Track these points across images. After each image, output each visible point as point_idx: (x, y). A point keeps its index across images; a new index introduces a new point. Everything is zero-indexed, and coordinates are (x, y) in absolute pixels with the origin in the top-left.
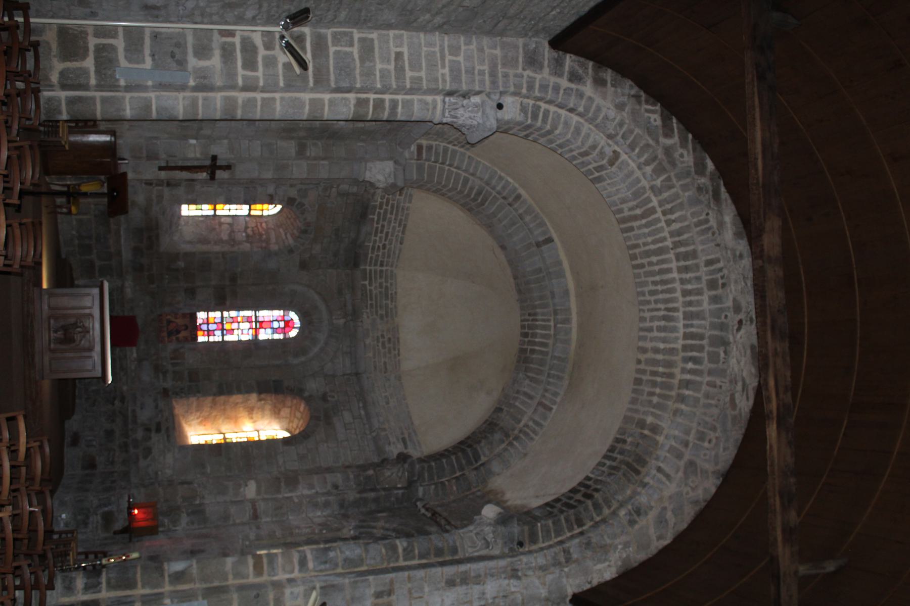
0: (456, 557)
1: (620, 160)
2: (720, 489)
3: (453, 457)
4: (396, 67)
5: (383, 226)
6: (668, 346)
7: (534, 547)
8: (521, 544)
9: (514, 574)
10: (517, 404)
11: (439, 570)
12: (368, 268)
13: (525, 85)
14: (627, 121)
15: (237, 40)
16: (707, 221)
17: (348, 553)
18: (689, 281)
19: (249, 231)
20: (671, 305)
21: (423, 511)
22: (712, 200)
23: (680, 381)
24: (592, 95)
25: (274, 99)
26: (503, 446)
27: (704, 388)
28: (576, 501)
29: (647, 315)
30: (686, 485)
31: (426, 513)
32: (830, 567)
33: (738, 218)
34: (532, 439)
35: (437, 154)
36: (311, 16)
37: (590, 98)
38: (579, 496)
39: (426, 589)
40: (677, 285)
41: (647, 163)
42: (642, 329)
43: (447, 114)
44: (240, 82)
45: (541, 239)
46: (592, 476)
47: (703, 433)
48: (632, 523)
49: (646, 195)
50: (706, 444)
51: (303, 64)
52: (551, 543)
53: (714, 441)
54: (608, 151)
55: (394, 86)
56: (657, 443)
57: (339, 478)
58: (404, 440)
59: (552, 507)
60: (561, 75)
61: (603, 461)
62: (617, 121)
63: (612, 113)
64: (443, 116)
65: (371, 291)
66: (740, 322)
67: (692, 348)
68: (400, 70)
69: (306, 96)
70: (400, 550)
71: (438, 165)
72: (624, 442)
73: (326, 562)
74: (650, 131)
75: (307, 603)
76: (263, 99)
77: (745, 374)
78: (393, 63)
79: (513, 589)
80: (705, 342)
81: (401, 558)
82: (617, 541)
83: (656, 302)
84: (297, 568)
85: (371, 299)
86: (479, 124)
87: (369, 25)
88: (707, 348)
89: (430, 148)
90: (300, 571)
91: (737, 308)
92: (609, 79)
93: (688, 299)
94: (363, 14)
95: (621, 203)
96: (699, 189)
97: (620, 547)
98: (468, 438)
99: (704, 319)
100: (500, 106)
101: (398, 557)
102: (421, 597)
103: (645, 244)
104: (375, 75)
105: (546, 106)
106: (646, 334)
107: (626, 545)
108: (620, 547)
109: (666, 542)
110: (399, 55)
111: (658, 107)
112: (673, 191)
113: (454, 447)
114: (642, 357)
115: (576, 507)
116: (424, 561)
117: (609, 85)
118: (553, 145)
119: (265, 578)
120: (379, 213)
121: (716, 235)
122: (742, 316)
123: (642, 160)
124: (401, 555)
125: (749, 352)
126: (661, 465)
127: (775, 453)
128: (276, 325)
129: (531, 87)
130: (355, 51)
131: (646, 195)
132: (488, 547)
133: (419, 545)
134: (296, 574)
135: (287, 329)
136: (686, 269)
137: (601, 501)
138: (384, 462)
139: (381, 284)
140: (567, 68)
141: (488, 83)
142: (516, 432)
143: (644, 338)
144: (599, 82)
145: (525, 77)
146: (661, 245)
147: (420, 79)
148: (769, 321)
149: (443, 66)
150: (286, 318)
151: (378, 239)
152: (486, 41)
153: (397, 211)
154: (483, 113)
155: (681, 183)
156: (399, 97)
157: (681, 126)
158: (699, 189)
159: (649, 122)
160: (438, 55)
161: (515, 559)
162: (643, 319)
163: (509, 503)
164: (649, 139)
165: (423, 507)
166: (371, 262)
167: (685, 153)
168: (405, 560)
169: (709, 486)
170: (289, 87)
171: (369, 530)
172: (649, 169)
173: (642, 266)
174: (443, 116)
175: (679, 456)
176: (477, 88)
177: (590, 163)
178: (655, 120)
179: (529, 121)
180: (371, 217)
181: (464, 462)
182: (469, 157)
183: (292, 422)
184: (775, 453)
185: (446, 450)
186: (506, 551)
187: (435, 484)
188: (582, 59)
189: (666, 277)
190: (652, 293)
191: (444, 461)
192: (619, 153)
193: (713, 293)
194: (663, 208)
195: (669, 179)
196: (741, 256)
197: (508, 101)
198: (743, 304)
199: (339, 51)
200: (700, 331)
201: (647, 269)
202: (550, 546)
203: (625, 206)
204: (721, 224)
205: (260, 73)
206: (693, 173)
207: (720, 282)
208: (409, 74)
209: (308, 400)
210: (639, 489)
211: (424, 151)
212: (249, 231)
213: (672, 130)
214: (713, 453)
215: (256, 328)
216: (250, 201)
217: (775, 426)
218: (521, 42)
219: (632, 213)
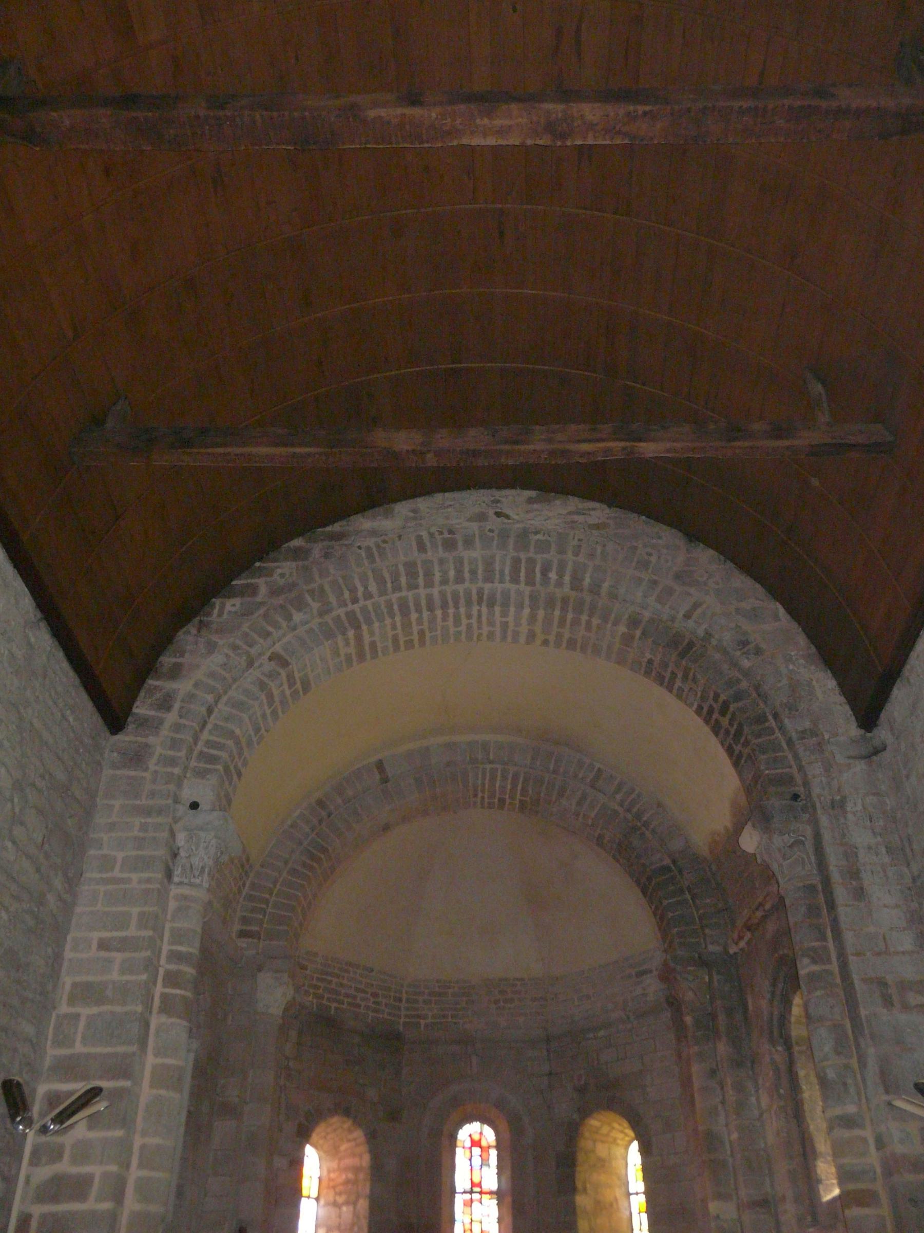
0: (820, 887)
1: (283, 653)
2: (709, 545)
3: (665, 903)
4: (118, 950)
5: (347, 996)
6: (527, 602)
7: (798, 779)
8: (796, 797)
9: (838, 805)
10: (593, 815)
11: (841, 911)
12: (402, 1020)
13: (169, 769)
14: (232, 640)
15: (37, 1210)
16: (368, 549)
17: (827, 1049)
18: (445, 573)
19: (340, 1200)
20: (475, 597)
21: (742, 944)
22: (341, 542)
23: (572, 589)
24: (192, 682)
25: (143, 1147)
26: (648, 834)
27: (581, 559)
28: (731, 724)
29: (485, 629)
30: (705, 584)
31: (746, 939)
32: (817, 388)
33: (366, 513)
34: (639, 795)
35: (253, 910)
36: (17, 1078)
37: (196, 685)
38: (725, 722)
39: (872, 929)
40: (448, 589)
41: (289, 617)
42: (504, 638)
43: (198, 881)
44: (107, 1206)
45: (378, 777)
46: (695, 706)
47: (638, 562)
48: (758, 651)
49: (330, 622)
50: (653, 559)
51: (94, 1093)
52: (790, 757)
53: (649, 550)
54: (269, 667)
55: (148, 953)
56: (651, 621)
57: (696, 1069)
58: (640, 974)
59: (740, 756)
60: (161, 722)
61: (675, 691)
62: (230, 653)
63: (218, 658)
64: (199, 886)
65: (434, 1016)
66: (498, 514)
67: (530, 572)
68: (125, 944)
69: (146, 1093)
70: (816, 968)
71: (270, 910)
72: (650, 662)
73: (845, 1084)
74: (247, 613)
75: (913, 1116)
76: (141, 1166)
77: (565, 512)
78: (114, 954)
79: (859, 807)
80: (523, 556)
81: (827, 967)
82: (784, 670)
83: (469, 616)
84: (857, 1132)
85: (444, 1016)
86: (215, 837)
87: (50, 987)
88: (531, 555)
89: (244, 920)
90: (862, 1126)
91: (481, 517)
92: (173, 660)
93: (467, 575)
94: (31, 996)
95: (339, 655)
96: (327, 556)
97: (791, 667)
98: (638, 882)
99: (493, 557)
100: (194, 806)
101: (827, 971)
102: (884, 938)
103: (394, 627)
104: (127, 982)
105: (200, 744)
106: (510, 633)
107: (788, 660)
108: (791, 667)
109: (781, 611)
110: (103, 945)
111: (217, 602)
112: (327, 587)
113: (651, 902)
114: (540, 637)
115: (740, 723)
116: (829, 934)
117: (180, 660)
118: (255, 739)
119: (879, 1187)
120: (329, 999)
121: (386, 538)
122: (491, 512)
123: (284, 624)
124: (824, 967)
125: (535, 506)
126: (682, 613)
127: (678, 445)
128: (477, 1161)
129: (173, 762)
130: (86, 1011)
131: (330, 622)
132: (802, 843)
133: (804, 939)
134: (867, 1133)
135: (484, 1143)
136: (428, 574)
137: (731, 692)
138: (674, 1003)
139: (425, 1002)
140: (152, 713)
141: (160, 820)
142: (629, 816)
143: (516, 634)
144: (175, 672)
145: (157, 768)
146: (396, 607)
147: (142, 915)
148: (508, 447)
149: (129, 880)
150: (468, 1144)
151: (363, 1004)
152: (100, 819)
153: (327, 974)
154: (201, 829)
155: (317, 578)
156: (166, 948)
157: (244, 575)
158: (327, 556)
159: (236, 612)
160: (110, 887)
161: (818, 805)
162: (491, 636)
163: (729, 825)
164: (256, 615)
165: (737, 944)
166: (394, 1015)
167: (279, 571)
168: (829, 961)
169: (705, 556)
170: (126, 1122)
171: (775, 1022)
172: (297, 617)
173: (422, 633)
174: (199, 886)
175: (670, 591)
176: (166, 834)
177: (283, 692)
178: (234, 605)
179: (220, 767)
180: (332, 1012)
181: (672, 888)
182: (262, 866)
183: (615, 1139)
184: (678, 445)
185: (655, 914)
186: (806, 816)
187: (702, 928)
188: (142, 694)
189: (437, 601)
190: (457, 622)
191: (670, 915)
192: (272, 653)
193: (460, 544)
194: (348, 601)
195: (311, 592)
196: (415, 511)
197: (188, 793)
198: (477, 510)
199: (84, 1038)
200: (508, 563)
201: (426, 626)
202: (796, 757)
203: (343, 651)
204: (373, 533)
205: (96, 1170)
206: (306, 563)
207: (446, 535)
208: (132, 931)
209: (585, 1112)
210: (714, 642)
211: (249, 928)
212: (340, 1200)
213: (248, 585)
214: (665, 551)
215: (481, 1193)
216: (296, 1193)
217: (642, 444)
218: (107, 772)
219: (352, 642)
